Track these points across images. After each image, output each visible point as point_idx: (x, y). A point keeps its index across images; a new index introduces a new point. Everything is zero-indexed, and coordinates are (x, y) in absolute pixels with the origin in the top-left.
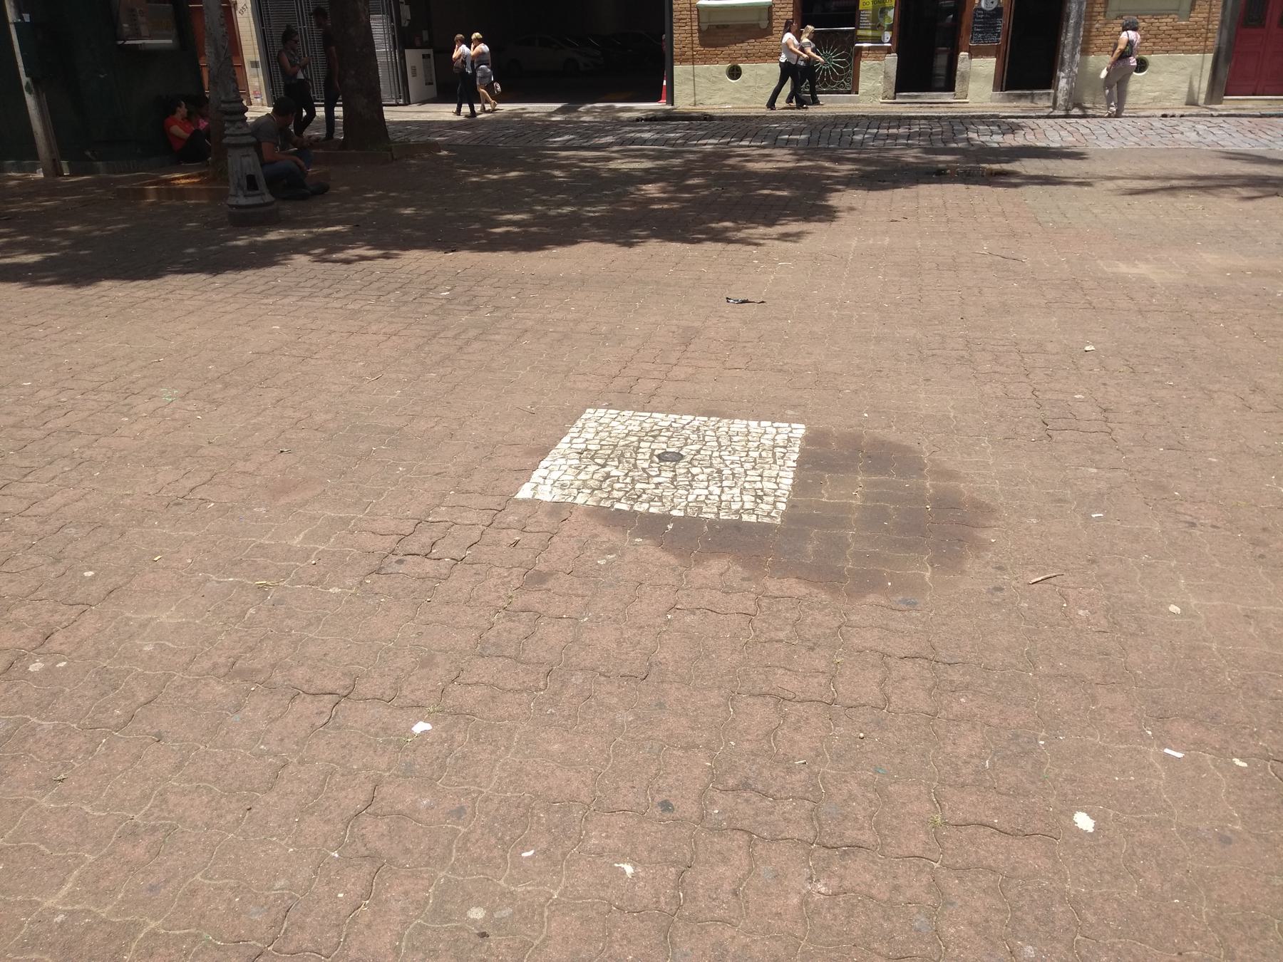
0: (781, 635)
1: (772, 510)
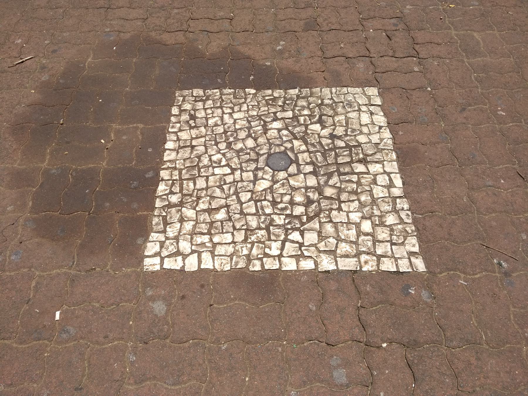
0: (176, 11)
1: (186, 100)
